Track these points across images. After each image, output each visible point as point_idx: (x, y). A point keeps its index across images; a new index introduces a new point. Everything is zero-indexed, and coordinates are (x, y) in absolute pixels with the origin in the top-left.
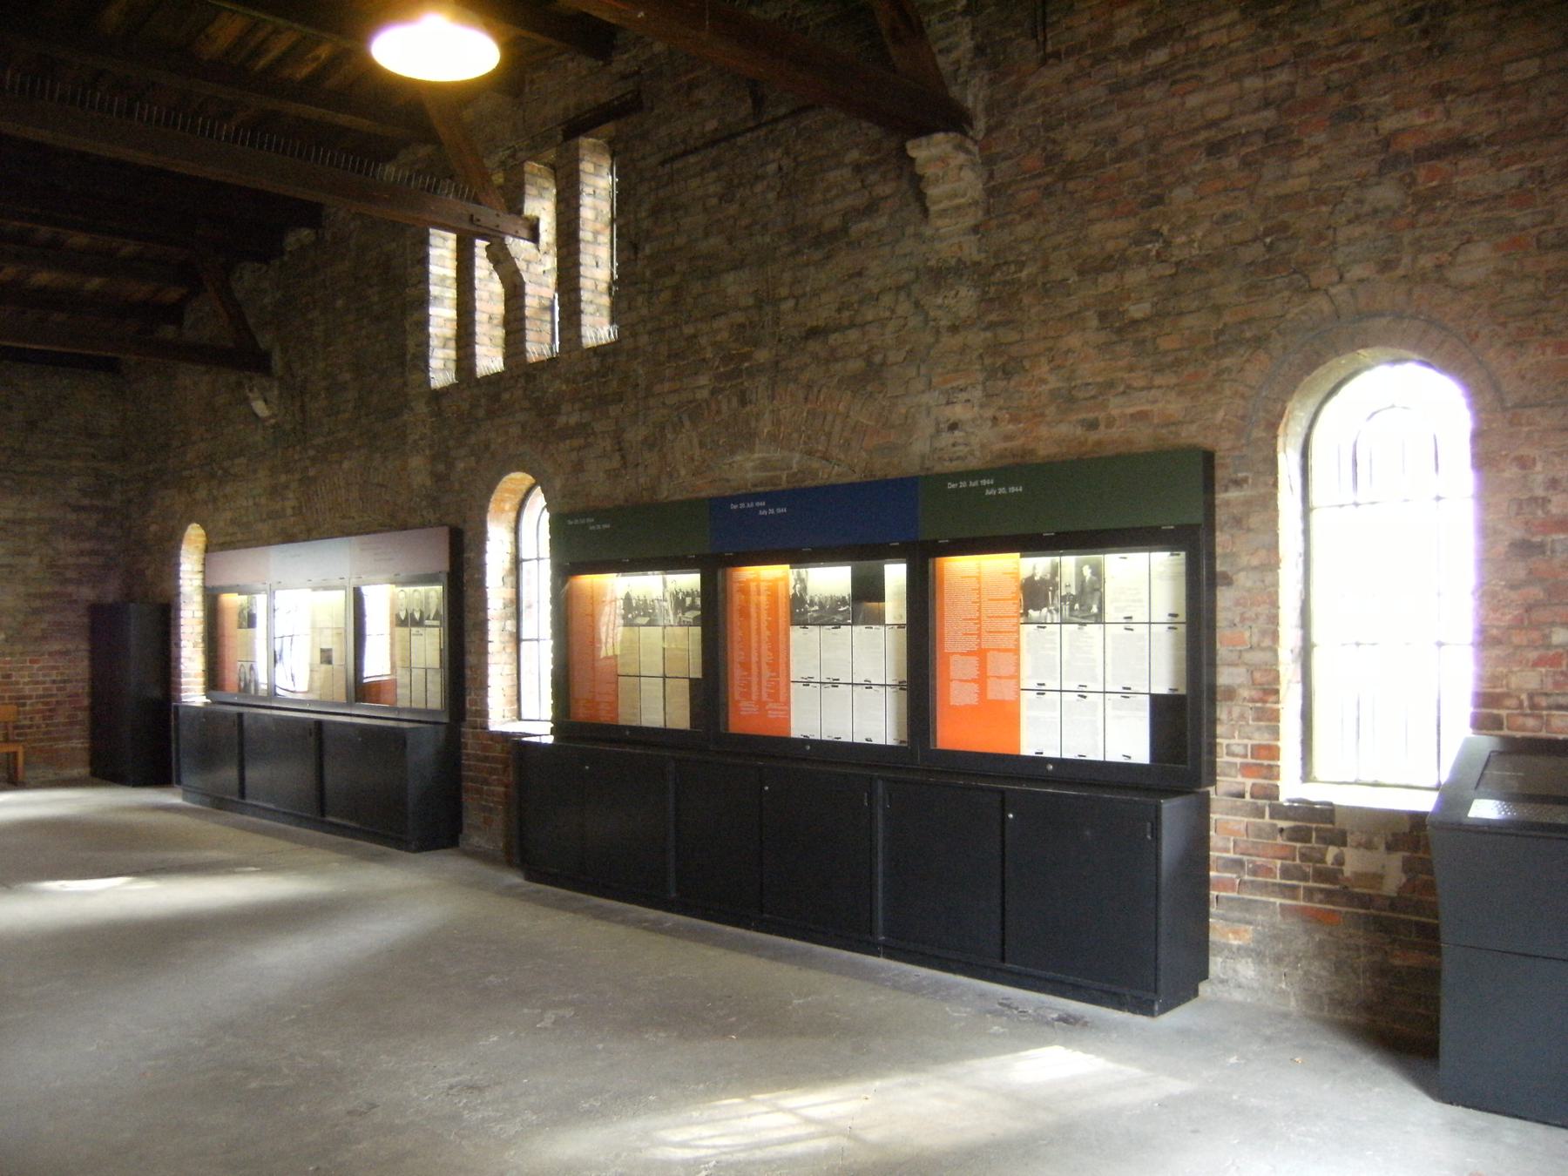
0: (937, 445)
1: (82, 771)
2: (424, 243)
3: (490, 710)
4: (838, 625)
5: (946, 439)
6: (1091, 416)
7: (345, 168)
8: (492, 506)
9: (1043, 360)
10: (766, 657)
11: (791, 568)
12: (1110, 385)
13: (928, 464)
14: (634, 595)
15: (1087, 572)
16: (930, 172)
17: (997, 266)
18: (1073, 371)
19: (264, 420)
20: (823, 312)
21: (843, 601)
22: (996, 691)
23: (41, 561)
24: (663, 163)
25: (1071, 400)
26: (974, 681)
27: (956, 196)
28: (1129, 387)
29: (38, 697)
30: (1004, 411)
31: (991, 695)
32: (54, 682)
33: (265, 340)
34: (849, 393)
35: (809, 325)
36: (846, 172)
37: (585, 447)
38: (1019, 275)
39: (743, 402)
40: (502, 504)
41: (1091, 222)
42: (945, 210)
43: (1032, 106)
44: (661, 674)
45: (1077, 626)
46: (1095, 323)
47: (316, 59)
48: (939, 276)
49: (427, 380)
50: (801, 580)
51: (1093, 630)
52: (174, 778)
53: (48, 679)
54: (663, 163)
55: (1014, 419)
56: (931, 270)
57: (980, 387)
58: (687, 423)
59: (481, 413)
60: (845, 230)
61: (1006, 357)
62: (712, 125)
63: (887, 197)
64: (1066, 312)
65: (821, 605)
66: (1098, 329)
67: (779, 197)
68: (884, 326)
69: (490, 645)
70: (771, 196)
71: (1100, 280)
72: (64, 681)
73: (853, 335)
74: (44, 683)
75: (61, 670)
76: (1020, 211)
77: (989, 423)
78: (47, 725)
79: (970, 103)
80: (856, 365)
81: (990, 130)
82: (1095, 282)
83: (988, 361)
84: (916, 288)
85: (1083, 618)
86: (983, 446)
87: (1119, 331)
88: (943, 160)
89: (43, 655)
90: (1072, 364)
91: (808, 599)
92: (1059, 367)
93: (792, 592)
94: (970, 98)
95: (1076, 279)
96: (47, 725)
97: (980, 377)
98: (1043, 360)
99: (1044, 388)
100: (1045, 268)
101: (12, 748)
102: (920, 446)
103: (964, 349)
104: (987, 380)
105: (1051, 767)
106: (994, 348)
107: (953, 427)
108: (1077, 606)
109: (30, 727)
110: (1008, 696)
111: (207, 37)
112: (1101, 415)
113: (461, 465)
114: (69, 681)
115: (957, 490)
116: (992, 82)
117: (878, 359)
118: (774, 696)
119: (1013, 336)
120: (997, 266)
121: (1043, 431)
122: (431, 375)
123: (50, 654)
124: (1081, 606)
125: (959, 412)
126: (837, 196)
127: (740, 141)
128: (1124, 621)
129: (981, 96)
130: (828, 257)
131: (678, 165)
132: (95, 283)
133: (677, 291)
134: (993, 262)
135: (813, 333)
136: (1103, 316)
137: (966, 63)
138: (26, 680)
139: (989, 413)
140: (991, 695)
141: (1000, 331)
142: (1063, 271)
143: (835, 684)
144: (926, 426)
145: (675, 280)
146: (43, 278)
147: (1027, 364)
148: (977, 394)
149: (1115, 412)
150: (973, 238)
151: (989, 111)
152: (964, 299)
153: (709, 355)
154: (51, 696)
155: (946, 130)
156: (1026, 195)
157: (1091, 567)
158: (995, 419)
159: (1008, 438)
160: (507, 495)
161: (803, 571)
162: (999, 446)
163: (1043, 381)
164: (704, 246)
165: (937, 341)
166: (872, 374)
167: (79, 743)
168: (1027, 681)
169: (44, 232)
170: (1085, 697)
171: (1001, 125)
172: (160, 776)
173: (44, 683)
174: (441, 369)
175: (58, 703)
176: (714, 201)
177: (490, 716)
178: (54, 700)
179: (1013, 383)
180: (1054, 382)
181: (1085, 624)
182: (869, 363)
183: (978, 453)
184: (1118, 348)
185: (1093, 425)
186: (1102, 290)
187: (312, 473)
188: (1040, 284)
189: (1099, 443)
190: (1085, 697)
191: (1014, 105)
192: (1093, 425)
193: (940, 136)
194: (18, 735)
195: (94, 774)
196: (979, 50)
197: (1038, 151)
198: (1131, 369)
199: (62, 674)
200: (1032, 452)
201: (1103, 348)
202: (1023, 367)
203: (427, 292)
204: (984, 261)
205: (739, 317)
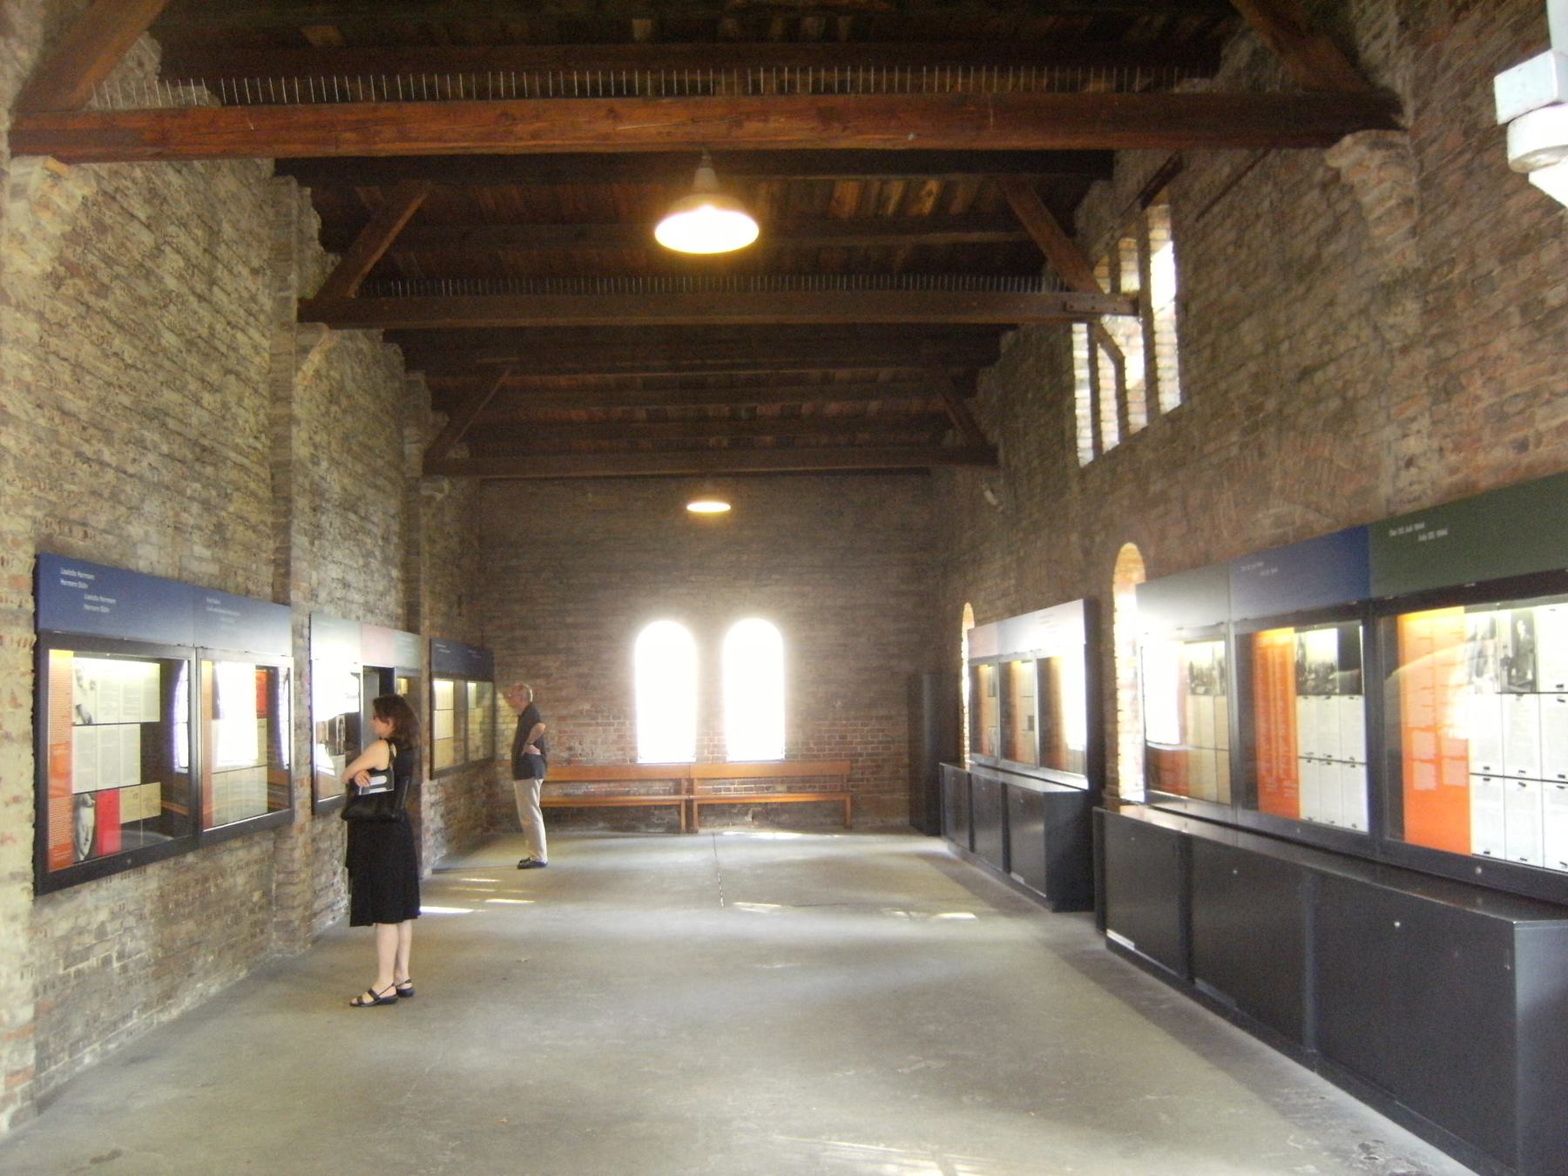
0: (1400, 485)
1: (902, 820)
2: (1070, 331)
3: (1120, 778)
4: (1329, 694)
5: (1407, 476)
6: (1520, 435)
7: (807, 289)
8: (1117, 578)
9: (1477, 372)
10: (1281, 733)
11: (1296, 631)
12: (1535, 394)
13: (1392, 508)
14: (1197, 664)
15: (1521, 629)
16: (1356, 179)
17: (1434, 271)
18: (1503, 382)
19: (996, 507)
20: (1309, 354)
21: (1331, 669)
22: (1451, 777)
23: (868, 639)
24: (1197, 220)
25: (1502, 417)
26: (1430, 761)
27: (1383, 200)
28: (1553, 394)
29: (868, 755)
30: (1448, 440)
31: (1447, 780)
32: (880, 742)
33: (994, 436)
34: (1330, 435)
35: (1303, 365)
36: (1315, 193)
37: (1166, 514)
38: (1450, 276)
39: (1262, 455)
40: (1128, 575)
41: (1507, 196)
42: (1379, 218)
43: (1450, 74)
44: (1213, 747)
45: (1514, 696)
46: (1516, 320)
47: (930, 194)
48: (1388, 292)
49: (1077, 461)
50: (1302, 646)
51: (1528, 699)
52: (537, 773)
53: (875, 740)
54: (1197, 220)
55: (1457, 448)
56: (1383, 285)
57: (1427, 414)
58: (1226, 483)
59: (1107, 487)
60: (1317, 257)
61: (1446, 376)
62: (1226, 170)
63: (1347, 212)
64: (1492, 313)
65: (1317, 672)
66: (1522, 327)
67: (1274, 234)
68: (1352, 356)
69: (1119, 714)
70: (1268, 233)
71: (1520, 266)
72: (888, 742)
73: (1331, 370)
74: (872, 743)
75: (887, 733)
76: (1447, 201)
77: (1436, 455)
78: (875, 779)
79: (1399, 88)
80: (1334, 404)
81: (1418, 113)
82: (1515, 268)
83: (1432, 382)
84: (1373, 310)
85: (1520, 686)
86: (1433, 483)
87: (1539, 326)
88: (1359, 164)
89: (871, 719)
90: (1502, 374)
91: (1307, 665)
92: (1490, 379)
93: (1296, 659)
94: (1399, 82)
95: (1500, 269)
96: (875, 779)
97: (1427, 402)
98: (1477, 372)
99: (1480, 406)
100: (1472, 265)
101: (842, 797)
102: (1385, 490)
103: (1414, 370)
104: (1434, 404)
105: (1479, 870)
106: (1437, 366)
107: (1410, 463)
108: (1514, 672)
109: (862, 780)
110: (1460, 782)
111: (837, 202)
112: (1530, 432)
113: (1098, 539)
114: (893, 742)
115: (1399, 537)
116: (1416, 58)
117: (1350, 394)
118: (1288, 773)
119: (1450, 350)
120: (1434, 271)
121: (1481, 459)
122: (1080, 454)
123: (877, 718)
124: (1518, 671)
125: (1413, 445)
126: (1312, 221)
127: (1244, 181)
128: (1557, 690)
129: (1408, 77)
130: (1309, 289)
131: (1208, 217)
132: (874, 405)
133: (1213, 346)
134: (1430, 266)
135: (1306, 373)
136: (1524, 310)
137: (1394, 43)
138: (859, 740)
139: (1435, 444)
140: (1447, 780)
141: (1441, 345)
142: (1490, 265)
143: (1328, 760)
144: (1389, 464)
145: (1208, 338)
146: (833, 408)
147: (1464, 381)
148: (1424, 423)
149: (1542, 427)
150: (1412, 242)
151: (1415, 95)
152: (1407, 315)
153: (1236, 410)
154: (877, 754)
155: (1353, 131)
156: (1452, 180)
157: (1525, 623)
158: (1441, 450)
159: (1453, 471)
160: (1131, 565)
161: (1303, 635)
162: (1447, 481)
163: (1477, 399)
164: (1227, 298)
165: (1393, 367)
166: (1346, 415)
167: (901, 796)
168: (1476, 766)
169: (815, 373)
170: (1524, 785)
171: (1426, 104)
172: (933, 829)
173: (872, 743)
174: (1086, 454)
175: (883, 760)
176: (1231, 250)
177: (1121, 784)
178: (881, 757)
179: (1453, 405)
180: (1488, 399)
181: (1520, 694)
182: (1344, 399)
183: (1429, 492)
184: (1541, 346)
185: (1522, 446)
186: (1523, 277)
187: (1022, 553)
188: (1469, 282)
189: (1530, 467)
190: (1524, 785)
191: (1435, 79)
192: (1522, 446)
193: (1348, 140)
194: (853, 786)
195: (912, 824)
196: (1404, 24)
197: (1457, 125)
198: (1553, 371)
199: (887, 736)
200: (1474, 484)
201: (1528, 348)
202: (1460, 384)
203: (1073, 377)
204: (1422, 267)
205: (1252, 367)
